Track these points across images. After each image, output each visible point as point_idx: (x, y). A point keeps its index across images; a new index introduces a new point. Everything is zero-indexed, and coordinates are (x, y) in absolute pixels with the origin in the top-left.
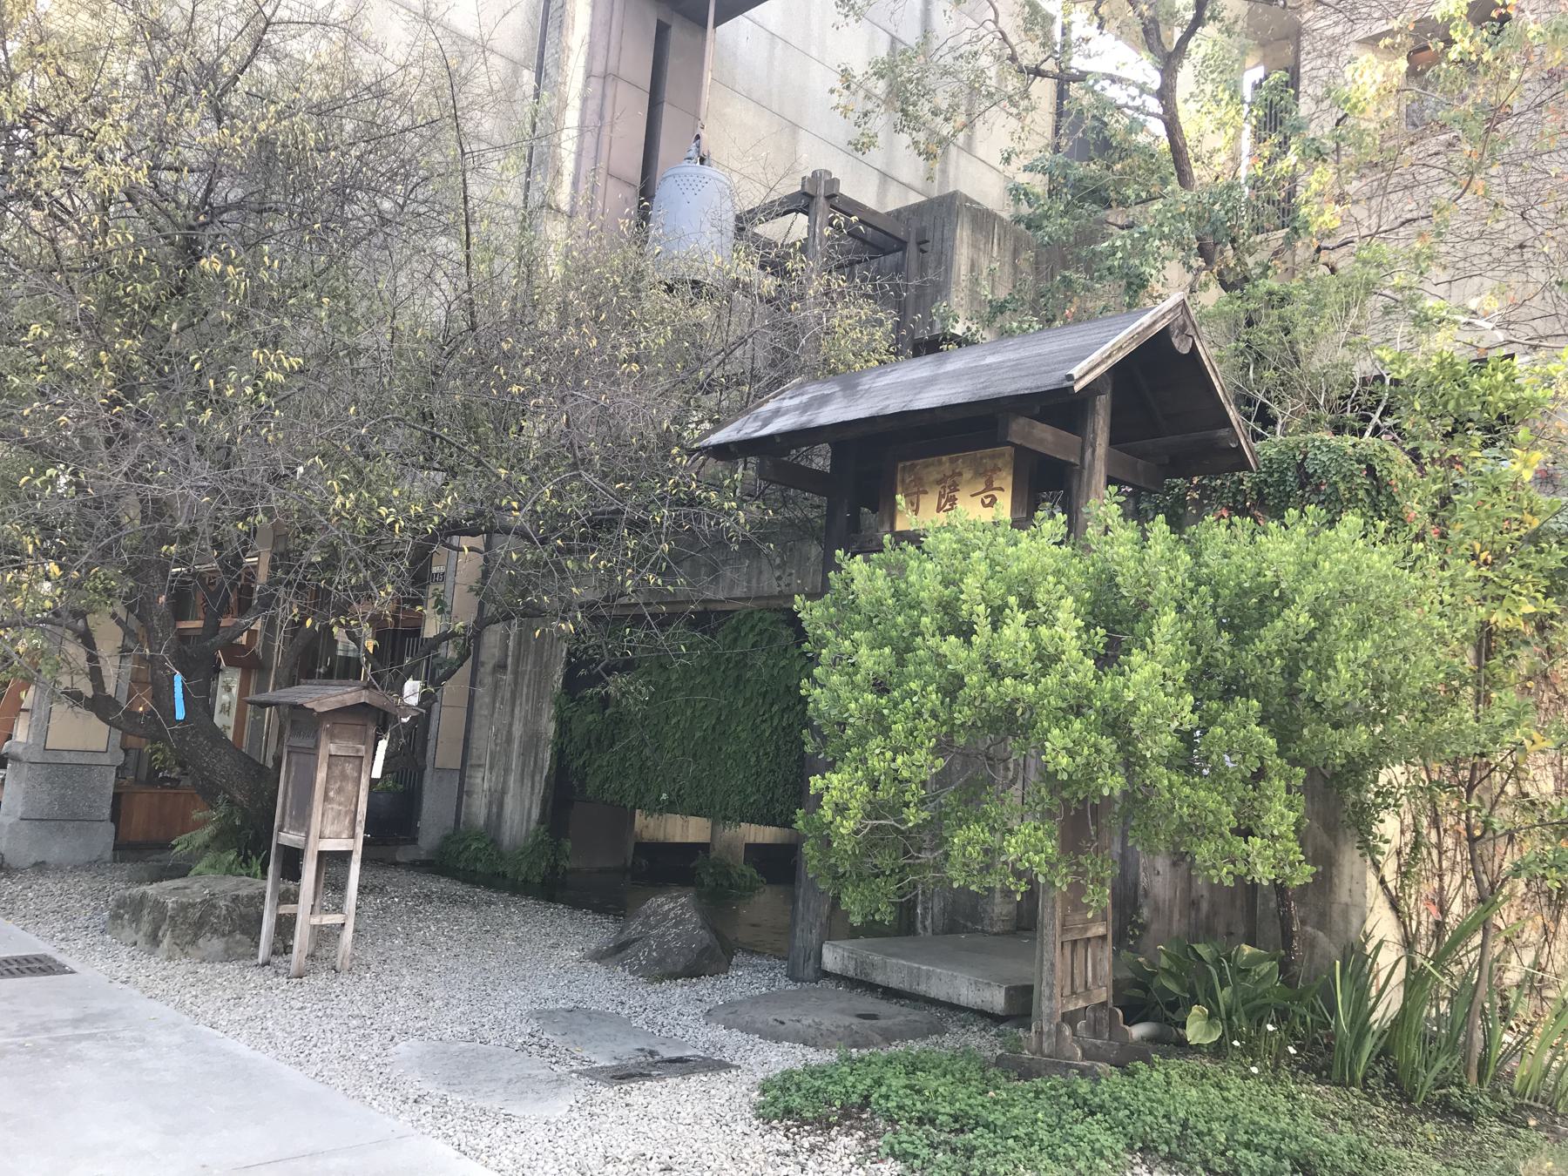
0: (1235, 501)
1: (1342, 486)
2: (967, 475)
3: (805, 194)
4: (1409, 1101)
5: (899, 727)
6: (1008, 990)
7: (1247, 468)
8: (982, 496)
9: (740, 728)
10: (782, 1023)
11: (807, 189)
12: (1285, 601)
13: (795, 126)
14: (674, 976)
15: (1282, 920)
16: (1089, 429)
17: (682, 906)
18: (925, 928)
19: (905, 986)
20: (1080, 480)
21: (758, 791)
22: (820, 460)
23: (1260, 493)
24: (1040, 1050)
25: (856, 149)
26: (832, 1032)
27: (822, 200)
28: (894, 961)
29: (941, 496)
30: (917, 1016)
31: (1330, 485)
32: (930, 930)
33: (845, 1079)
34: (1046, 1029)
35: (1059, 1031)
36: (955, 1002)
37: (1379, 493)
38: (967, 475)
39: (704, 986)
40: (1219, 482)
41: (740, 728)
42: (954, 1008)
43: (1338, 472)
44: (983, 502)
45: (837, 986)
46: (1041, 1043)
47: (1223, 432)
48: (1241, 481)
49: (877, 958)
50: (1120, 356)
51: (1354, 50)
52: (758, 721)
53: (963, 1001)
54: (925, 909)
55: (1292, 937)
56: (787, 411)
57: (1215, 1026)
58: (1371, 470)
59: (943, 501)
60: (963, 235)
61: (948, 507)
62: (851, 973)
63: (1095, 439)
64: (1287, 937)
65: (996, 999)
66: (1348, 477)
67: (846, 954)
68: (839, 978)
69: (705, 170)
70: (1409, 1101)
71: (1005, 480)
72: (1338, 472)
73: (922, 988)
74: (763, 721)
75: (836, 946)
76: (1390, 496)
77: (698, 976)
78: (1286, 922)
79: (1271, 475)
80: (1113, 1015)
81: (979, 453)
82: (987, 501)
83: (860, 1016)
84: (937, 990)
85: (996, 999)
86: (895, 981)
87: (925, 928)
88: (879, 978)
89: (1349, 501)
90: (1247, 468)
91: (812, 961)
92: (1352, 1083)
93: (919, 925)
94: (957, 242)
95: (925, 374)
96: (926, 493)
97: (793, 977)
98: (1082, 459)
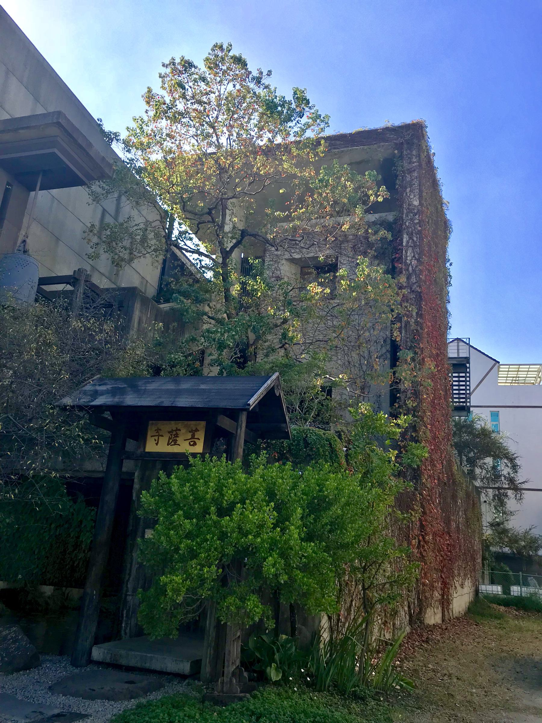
0: (280, 450)
1: (321, 450)
2: (183, 431)
3: (75, 278)
4: (343, 695)
5: (203, 555)
6: (191, 663)
7: (288, 438)
8: (190, 441)
9: (30, 535)
10: (94, 690)
11: (76, 276)
12: (330, 504)
13: (58, 239)
14: (18, 670)
15: (292, 622)
16: (240, 421)
17: (15, 631)
18: (126, 634)
19: (139, 665)
20: (235, 440)
21: (37, 567)
22: (107, 415)
23: (289, 448)
24: (222, 691)
25: (89, 258)
26: (121, 692)
27: (83, 282)
28: (133, 653)
29: (170, 439)
30: (153, 678)
31: (316, 449)
32: (128, 635)
33: (159, 715)
34: (225, 681)
35: (231, 681)
36: (165, 670)
37: (332, 453)
38: (183, 431)
39: (34, 674)
40: (274, 442)
41: (30, 535)
42: (161, 673)
43: (319, 444)
44: (190, 443)
45: (98, 668)
46: (223, 688)
47: (284, 425)
48: (283, 442)
49: (123, 652)
50: (262, 396)
51: (284, 262)
52: (42, 532)
53: (169, 670)
54: (126, 624)
55: (296, 630)
56: (102, 393)
57: (279, 672)
58: (330, 444)
59: (171, 441)
60: (137, 306)
61: (173, 443)
62: (108, 660)
63: (242, 424)
64: (293, 629)
65: (186, 667)
66: (323, 446)
67: (106, 651)
68: (98, 663)
69: (24, 256)
70: (343, 695)
71: (201, 435)
72: (319, 444)
73: (147, 665)
74: (45, 532)
75: (100, 648)
76: (336, 455)
77: (29, 669)
78: (293, 623)
79: (294, 442)
80: (241, 670)
81: (189, 423)
82: (192, 443)
83: (126, 682)
84: (156, 665)
85: (186, 667)
86: (133, 663)
87: (126, 634)
88: (124, 662)
89: (323, 455)
90: (288, 438)
91: (86, 656)
92: (324, 691)
93: (123, 632)
94: (135, 309)
95: (172, 388)
96: (162, 436)
97: (75, 664)
98: (237, 432)
